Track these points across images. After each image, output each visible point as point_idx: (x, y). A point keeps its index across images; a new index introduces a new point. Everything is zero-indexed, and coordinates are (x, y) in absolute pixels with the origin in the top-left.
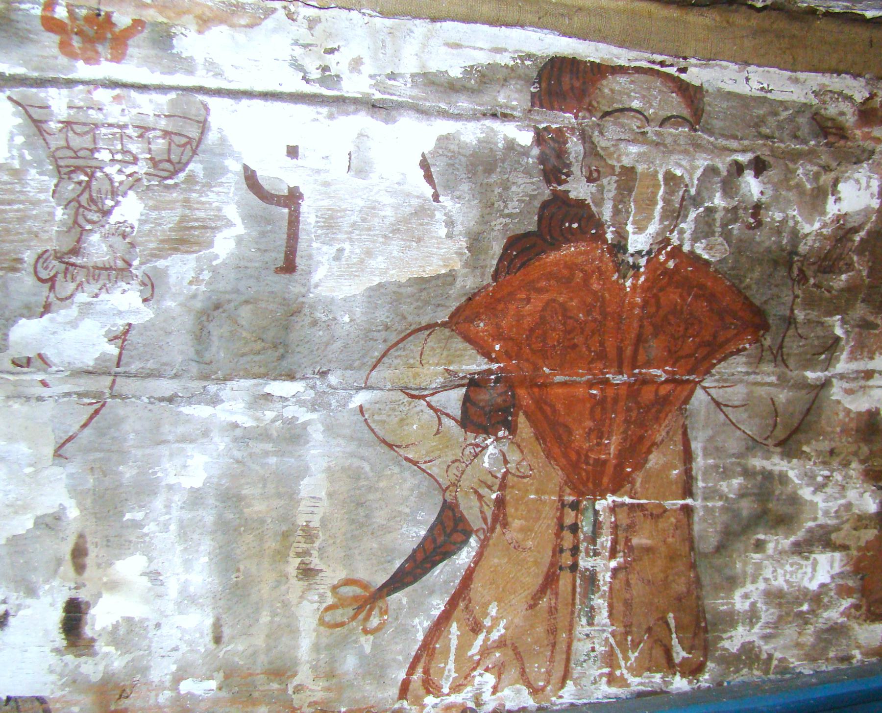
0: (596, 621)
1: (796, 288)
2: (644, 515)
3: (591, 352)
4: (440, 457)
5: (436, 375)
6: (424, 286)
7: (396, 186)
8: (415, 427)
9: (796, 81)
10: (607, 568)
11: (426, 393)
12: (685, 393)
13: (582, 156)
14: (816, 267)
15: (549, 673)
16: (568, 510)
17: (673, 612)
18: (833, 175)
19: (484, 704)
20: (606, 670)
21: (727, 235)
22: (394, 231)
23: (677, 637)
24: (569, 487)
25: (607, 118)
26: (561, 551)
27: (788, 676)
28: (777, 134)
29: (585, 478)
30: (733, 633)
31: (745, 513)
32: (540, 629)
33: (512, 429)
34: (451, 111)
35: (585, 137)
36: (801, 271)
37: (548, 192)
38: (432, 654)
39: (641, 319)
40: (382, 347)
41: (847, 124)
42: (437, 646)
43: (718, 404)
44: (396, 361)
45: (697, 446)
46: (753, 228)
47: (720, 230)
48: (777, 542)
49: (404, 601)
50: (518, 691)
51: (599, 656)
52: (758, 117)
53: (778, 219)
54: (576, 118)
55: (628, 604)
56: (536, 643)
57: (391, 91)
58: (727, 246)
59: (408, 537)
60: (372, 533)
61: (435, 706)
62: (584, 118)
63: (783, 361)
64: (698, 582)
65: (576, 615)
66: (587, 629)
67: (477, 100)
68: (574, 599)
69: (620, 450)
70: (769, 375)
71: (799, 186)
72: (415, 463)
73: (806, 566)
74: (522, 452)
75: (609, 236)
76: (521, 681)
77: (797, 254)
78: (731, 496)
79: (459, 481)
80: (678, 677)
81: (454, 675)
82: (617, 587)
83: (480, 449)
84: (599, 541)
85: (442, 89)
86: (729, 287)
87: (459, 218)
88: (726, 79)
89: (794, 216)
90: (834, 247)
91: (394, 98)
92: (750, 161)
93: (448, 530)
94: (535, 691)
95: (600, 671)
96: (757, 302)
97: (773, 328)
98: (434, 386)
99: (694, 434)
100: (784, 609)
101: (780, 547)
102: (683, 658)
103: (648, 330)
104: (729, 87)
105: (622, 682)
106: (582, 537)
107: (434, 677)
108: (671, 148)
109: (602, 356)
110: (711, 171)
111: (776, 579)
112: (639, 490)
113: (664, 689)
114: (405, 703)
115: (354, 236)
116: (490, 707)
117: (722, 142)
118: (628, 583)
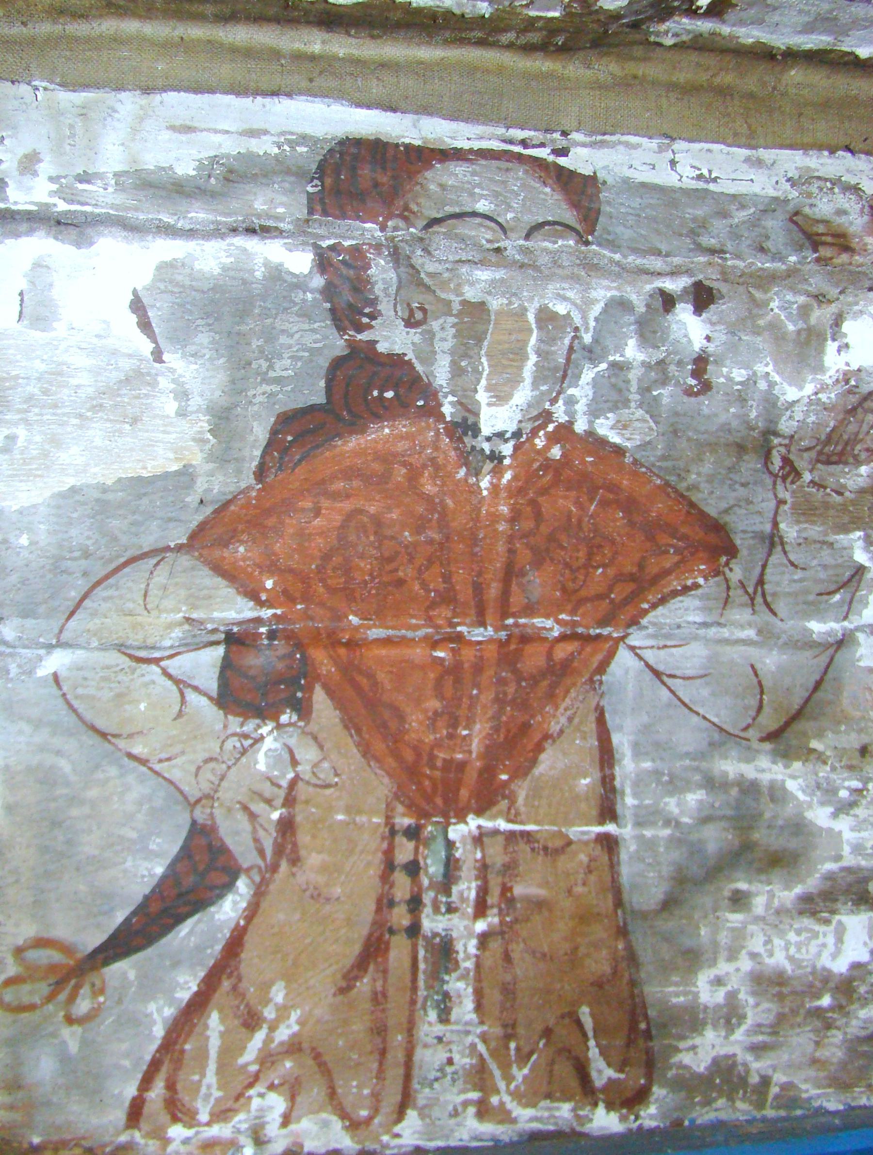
0: (453, 1016)
1: (780, 487)
2: (533, 849)
3: (428, 591)
4: (183, 753)
5: (170, 626)
6: (143, 491)
7: (95, 340)
8: (142, 706)
9: (759, 163)
10: (470, 934)
11: (157, 654)
12: (599, 657)
13: (395, 287)
14: (813, 454)
15: (376, 1096)
16: (400, 840)
17: (590, 1005)
18: (833, 308)
19: (269, 1142)
20: (474, 1095)
21: (651, 406)
22: (98, 408)
23: (598, 1045)
24: (402, 803)
25: (436, 228)
26: (391, 904)
27: (799, 1112)
28: (729, 246)
29: (429, 790)
30: (698, 1041)
31: (712, 847)
32: (359, 1027)
33: (303, 709)
34: (179, 225)
35: (396, 256)
36: (786, 461)
37: (341, 343)
38: (178, 1063)
39: (511, 539)
40: (83, 585)
41: (852, 230)
42: (187, 1047)
43: (657, 674)
44: (105, 606)
45: (621, 740)
46: (697, 394)
47: (638, 397)
48: (771, 895)
49: (132, 975)
50: (325, 1124)
51: (461, 1072)
52: (694, 220)
53: (738, 379)
54: (383, 228)
55: (508, 991)
56: (352, 1048)
57: (82, 199)
58: (652, 424)
59: (135, 875)
60: (78, 869)
61: (186, 1141)
62: (396, 229)
63: (767, 604)
64: (632, 958)
65: (419, 1005)
66: (439, 1029)
67: (220, 207)
68: (414, 980)
69: (487, 747)
70: (742, 627)
71: (775, 327)
72: (143, 762)
73: (825, 935)
74: (321, 747)
75: (447, 410)
76: (330, 1107)
77: (776, 434)
78: (686, 820)
79: (216, 791)
80: (601, 1110)
81: (217, 1094)
82: (488, 963)
83: (250, 741)
84: (455, 889)
85: (164, 193)
86: (658, 487)
87: (194, 386)
88: (636, 164)
89: (767, 374)
90: (842, 423)
91: (88, 209)
92: (685, 290)
93: (201, 867)
94: (354, 1125)
95: (463, 1097)
96: (712, 511)
97: (744, 552)
98: (167, 643)
99: (618, 721)
100: (787, 1002)
101: (776, 902)
102: (610, 1079)
103: (524, 556)
104: (644, 176)
105: (504, 1116)
106: (426, 882)
107: (184, 1096)
108: (547, 272)
109: (448, 598)
110: (621, 305)
111: (771, 955)
112: (522, 809)
113: (578, 1129)
114: (137, 1135)
115: (31, 416)
116: (280, 1146)
117: (633, 260)
118: (507, 957)
